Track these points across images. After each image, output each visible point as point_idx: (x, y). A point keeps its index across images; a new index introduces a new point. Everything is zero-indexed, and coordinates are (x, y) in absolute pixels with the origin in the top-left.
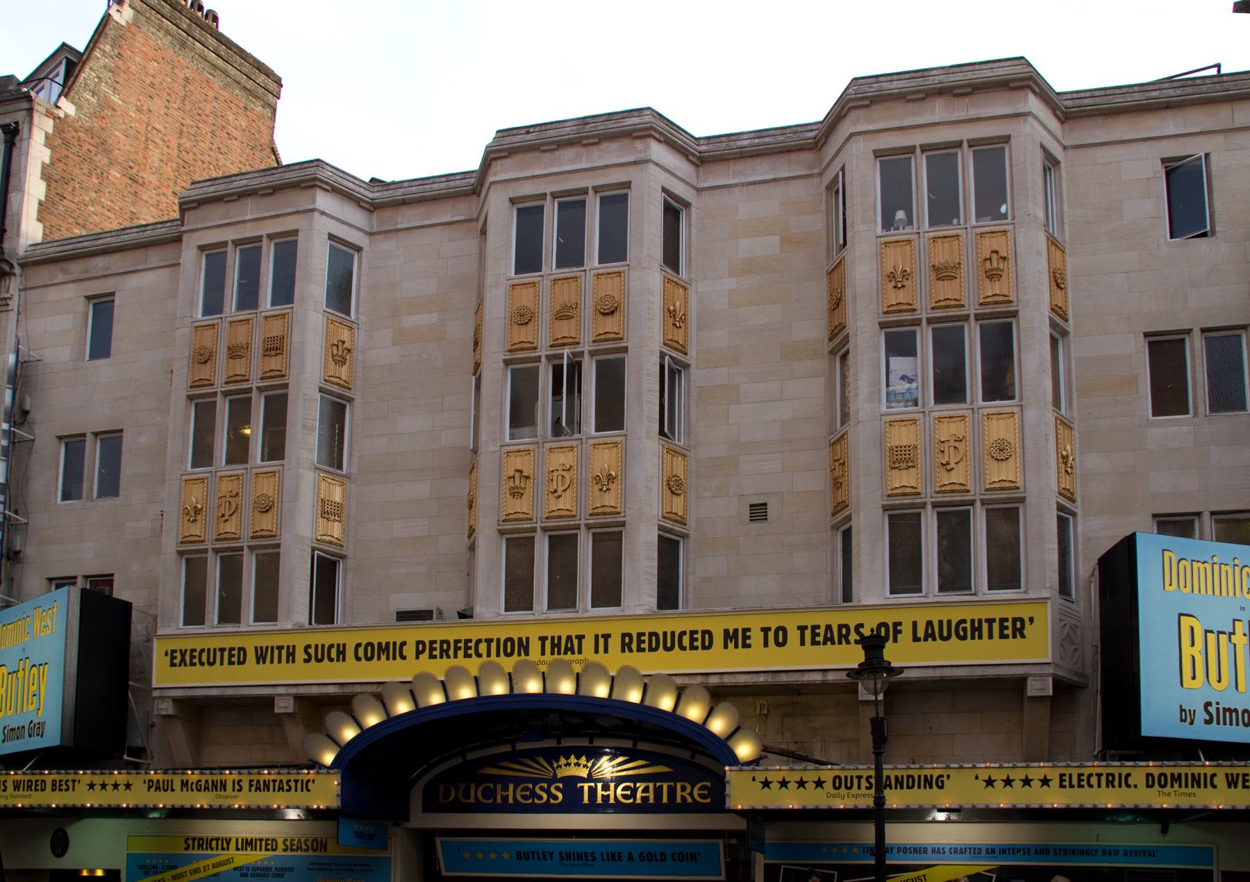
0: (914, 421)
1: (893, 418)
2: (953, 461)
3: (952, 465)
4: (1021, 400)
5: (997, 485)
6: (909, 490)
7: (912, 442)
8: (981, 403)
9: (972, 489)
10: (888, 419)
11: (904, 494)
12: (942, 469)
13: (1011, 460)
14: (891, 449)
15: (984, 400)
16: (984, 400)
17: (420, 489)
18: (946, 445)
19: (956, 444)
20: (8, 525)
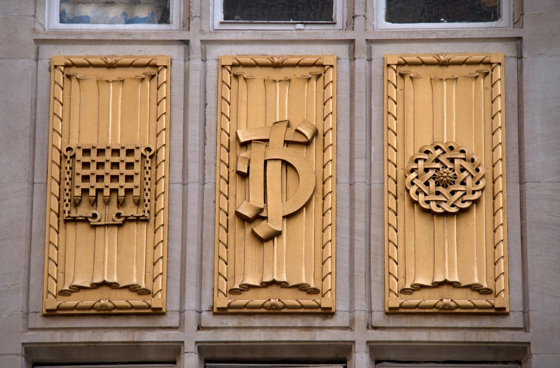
0: (152, 69)
1: (78, 54)
2: (276, 210)
3: (275, 223)
4: (518, 22)
5: (429, 299)
6: (121, 299)
7: (141, 139)
8: (382, 24)
9: (341, 307)
10: (62, 54)
11: (105, 313)
12: (240, 235)
13: (479, 219)
14: (68, 156)
15: (391, 17)
16: (391, 17)
17: (107, 232)
18: (257, 154)
19: (290, 154)
20: (140, 3)
